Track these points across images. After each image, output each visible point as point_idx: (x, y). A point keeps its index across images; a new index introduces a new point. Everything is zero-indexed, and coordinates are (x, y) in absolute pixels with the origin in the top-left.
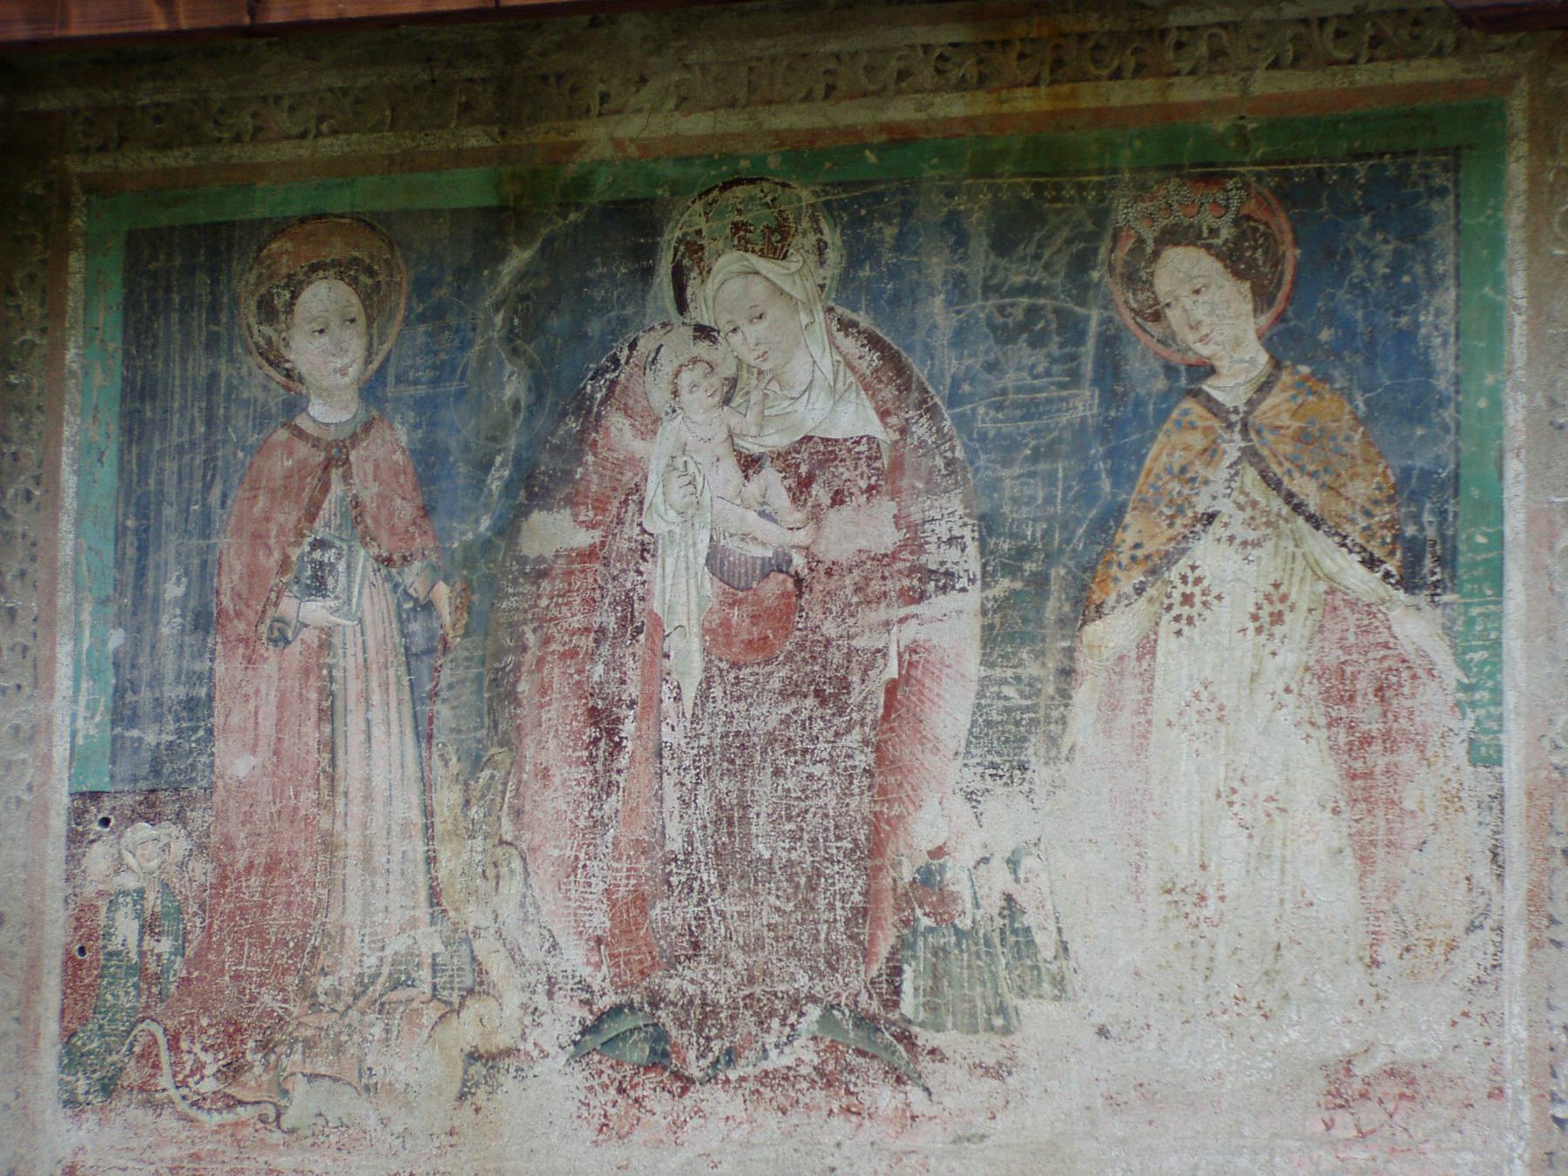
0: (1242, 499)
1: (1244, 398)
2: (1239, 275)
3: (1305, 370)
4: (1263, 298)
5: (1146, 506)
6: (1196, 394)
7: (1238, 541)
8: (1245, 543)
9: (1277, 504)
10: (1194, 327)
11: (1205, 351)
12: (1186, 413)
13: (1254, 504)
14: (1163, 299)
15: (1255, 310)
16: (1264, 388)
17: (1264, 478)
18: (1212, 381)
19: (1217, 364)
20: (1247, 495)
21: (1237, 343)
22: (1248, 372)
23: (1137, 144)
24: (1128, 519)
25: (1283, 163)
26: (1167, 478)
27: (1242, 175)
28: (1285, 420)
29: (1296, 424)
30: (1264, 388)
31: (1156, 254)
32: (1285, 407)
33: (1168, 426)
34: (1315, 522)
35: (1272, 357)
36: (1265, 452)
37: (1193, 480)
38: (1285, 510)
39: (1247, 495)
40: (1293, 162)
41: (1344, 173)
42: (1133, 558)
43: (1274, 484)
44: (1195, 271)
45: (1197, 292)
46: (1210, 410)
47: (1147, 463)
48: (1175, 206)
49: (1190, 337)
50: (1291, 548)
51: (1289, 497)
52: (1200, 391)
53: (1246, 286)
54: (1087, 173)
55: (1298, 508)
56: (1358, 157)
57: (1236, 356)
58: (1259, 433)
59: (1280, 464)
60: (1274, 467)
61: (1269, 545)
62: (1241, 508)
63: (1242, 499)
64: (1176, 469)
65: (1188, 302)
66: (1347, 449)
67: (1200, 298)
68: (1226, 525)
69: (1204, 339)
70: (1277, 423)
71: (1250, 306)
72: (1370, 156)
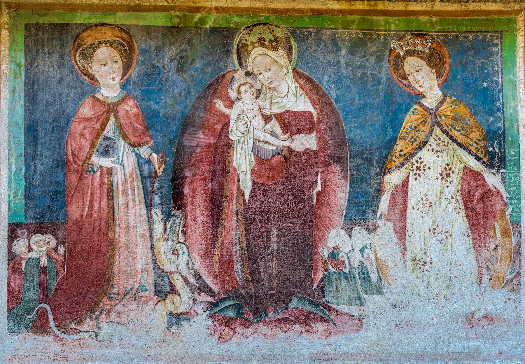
0: (435, 137)
1: (435, 105)
3: (454, 98)
4: (439, 75)
5: (403, 138)
6: (419, 104)
7: (435, 150)
9: (447, 139)
10: (418, 82)
11: (421, 90)
12: (415, 109)
13: (440, 139)
14: (407, 73)
15: (437, 78)
16: (442, 103)
17: (442, 131)
19: (425, 94)
20: (437, 136)
21: (431, 88)
22: (436, 97)
23: (397, 22)
24: (398, 142)
25: (445, 32)
26: (410, 129)
28: (449, 113)
30: (442, 103)
31: (404, 59)
32: (448, 109)
33: (410, 113)
34: (461, 145)
35: (443, 93)
38: (450, 141)
39: (437, 136)
41: (465, 37)
43: (446, 133)
44: (417, 65)
45: (418, 71)
47: (404, 124)
49: (416, 86)
50: (453, 153)
51: (451, 138)
52: (421, 103)
54: (381, 31)
55: (454, 141)
57: (431, 92)
58: (440, 117)
59: (448, 127)
60: (446, 128)
61: (445, 152)
62: (436, 140)
63: (435, 137)
64: (413, 127)
65: (415, 74)
68: (431, 145)
69: (421, 86)
70: (446, 114)
72: (473, 32)
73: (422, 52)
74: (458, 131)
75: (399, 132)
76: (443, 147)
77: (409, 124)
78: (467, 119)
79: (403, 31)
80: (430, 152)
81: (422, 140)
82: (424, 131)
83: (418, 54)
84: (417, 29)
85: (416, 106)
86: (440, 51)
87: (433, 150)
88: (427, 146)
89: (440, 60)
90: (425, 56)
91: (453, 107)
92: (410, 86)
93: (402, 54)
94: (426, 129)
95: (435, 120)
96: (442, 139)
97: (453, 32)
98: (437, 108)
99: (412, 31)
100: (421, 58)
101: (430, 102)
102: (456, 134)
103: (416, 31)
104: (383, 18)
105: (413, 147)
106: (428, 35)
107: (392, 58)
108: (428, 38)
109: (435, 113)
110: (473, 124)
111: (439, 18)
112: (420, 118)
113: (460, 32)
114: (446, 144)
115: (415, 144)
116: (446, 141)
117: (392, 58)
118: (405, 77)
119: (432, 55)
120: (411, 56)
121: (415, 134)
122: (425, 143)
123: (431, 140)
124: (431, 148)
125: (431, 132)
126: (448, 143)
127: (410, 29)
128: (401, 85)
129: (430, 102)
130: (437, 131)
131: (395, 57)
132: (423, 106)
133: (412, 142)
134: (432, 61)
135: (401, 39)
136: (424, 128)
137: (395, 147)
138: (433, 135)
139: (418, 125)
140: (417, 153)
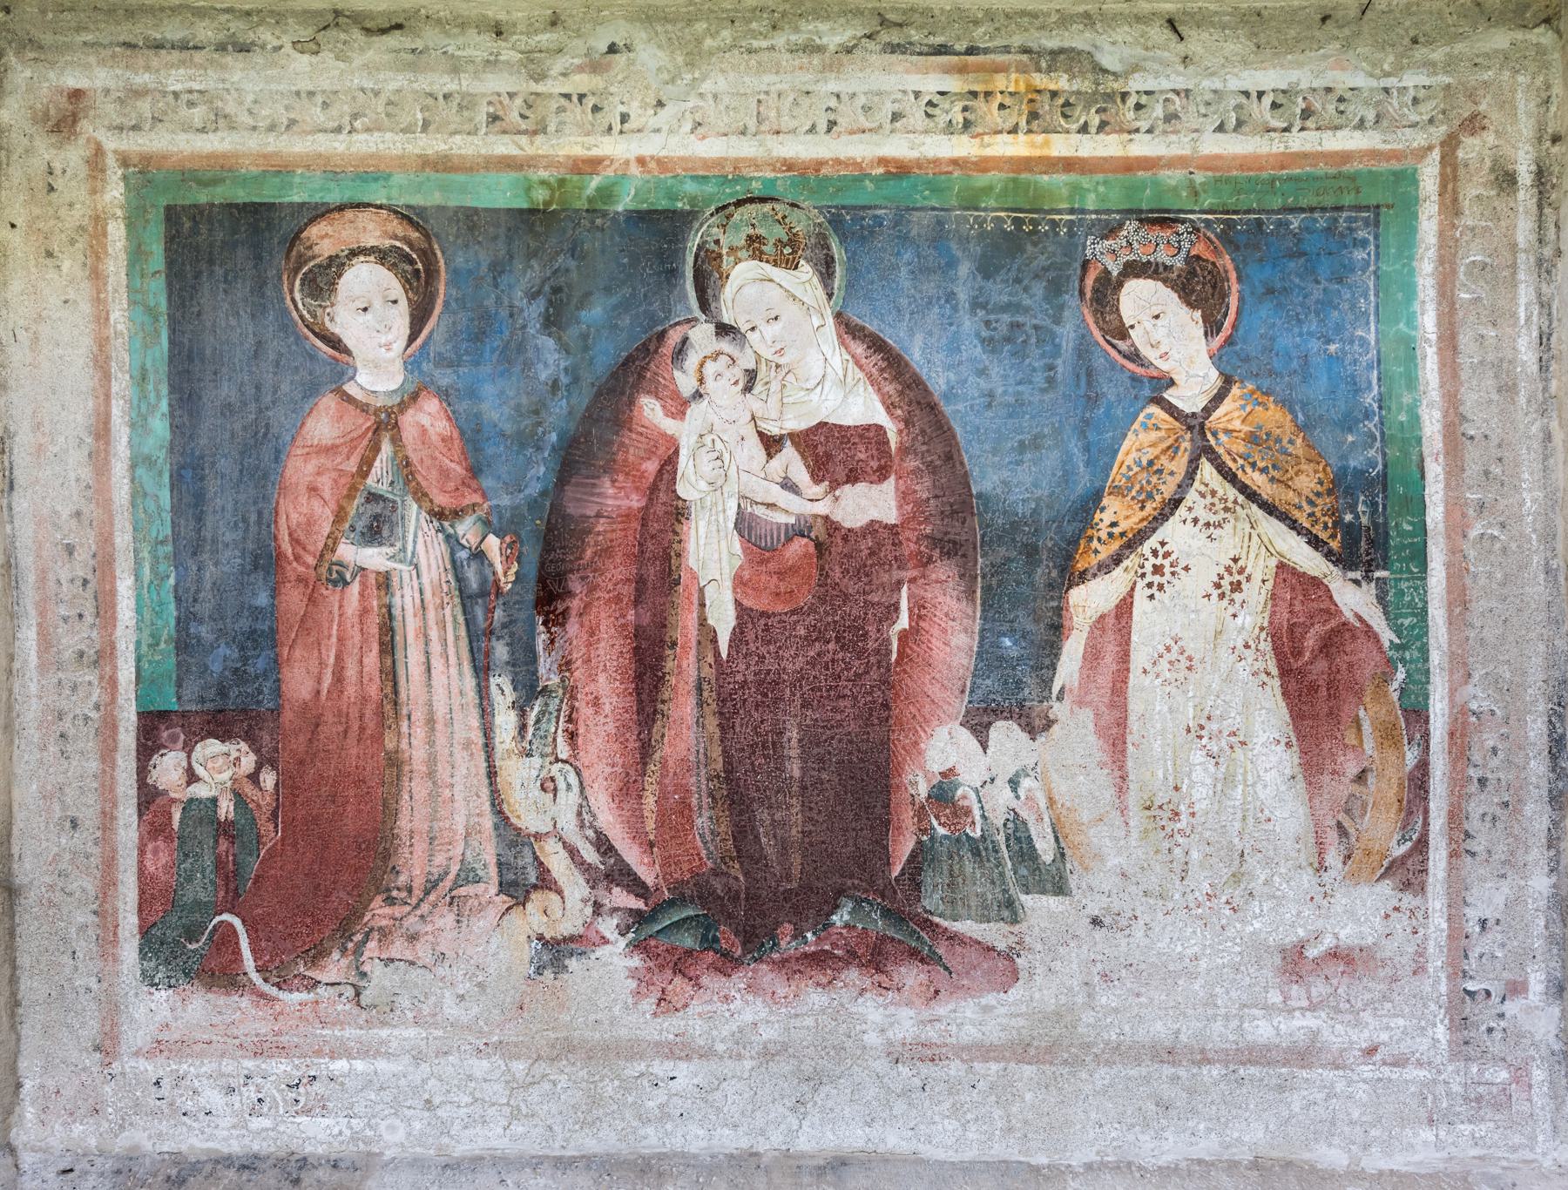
0: (1203, 489)
2: (1192, 305)
4: (1212, 327)
5: (1117, 491)
6: (1159, 401)
8: (1208, 525)
9: (1232, 493)
11: (1164, 366)
12: (1149, 416)
13: (1213, 493)
14: (1128, 323)
15: (1206, 334)
16: (1218, 399)
18: (1170, 391)
23: (1101, 189)
24: (1105, 502)
25: (1227, 213)
26: (1136, 469)
27: (1191, 221)
28: (1237, 424)
29: (1247, 429)
30: (1218, 399)
31: (1120, 285)
32: (1236, 414)
33: (1136, 426)
34: (1270, 509)
36: (1221, 451)
37: (1160, 472)
38: (1241, 498)
40: (1235, 212)
41: (1279, 224)
42: (1111, 535)
45: (1157, 317)
46: (1171, 415)
47: (1120, 456)
48: (1135, 245)
50: (1248, 529)
51: (1244, 489)
52: (1163, 399)
53: (1198, 314)
54: (1059, 212)
55: (1252, 495)
56: (1292, 210)
58: (1215, 435)
59: (1234, 460)
60: (1230, 464)
61: (1227, 527)
62: (1203, 496)
63: (1203, 489)
64: (1144, 463)
66: (1291, 449)
67: (1158, 322)
68: (1190, 509)
71: (1202, 331)
72: (1302, 210)
73: (1166, 267)
74: (1263, 470)
75: (1108, 476)
76: (1222, 515)
77: (1134, 455)
78: (1285, 441)
79: (1118, 212)
80: (1189, 524)
81: (1167, 496)
82: (1172, 473)
83: (1156, 272)
84: (1154, 206)
85: (1153, 409)
86: (1213, 264)
87: (1196, 521)
88: (1182, 511)
89: (1214, 287)
90: (1174, 276)
91: (1248, 409)
92: (1135, 356)
93: (1115, 274)
94: (1180, 465)
95: (1200, 443)
96: (1220, 493)
97: (1248, 212)
98: (1207, 411)
99: (1141, 211)
100: (1165, 281)
101: (1190, 395)
102: (1256, 480)
103: (1152, 211)
104: (1064, 177)
105: (1144, 513)
106: (1183, 222)
107: (1090, 282)
108: (1181, 228)
109: (1202, 426)
110: (1300, 452)
111: (1210, 174)
112: (1161, 440)
113: (1268, 212)
114: (1230, 505)
115: (1149, 506)
116: (1231, 498)
117: (1090, 282)
118: (1123, 333)
119: (1192, 273)
120: (1138, 276)
121: (1149, 482)
122: (1176, 503)
123: (1191, 496)
124: (1190, 517)
125: (1191, 475)
126: (1235, 502)
127: (1134, 207)
128: (1109, 348)
129: (1190, 395)
130: (1207, 470)
131: (1097, 280)
132: (1171, 410)
133: (1143, 502)
134: (1193, 291)
135: (1111, 231)
136: (1172, 466)
137: (1098, 516)
138: (1196, 484)
139: (1157, 457)
140: (1154, 530)
